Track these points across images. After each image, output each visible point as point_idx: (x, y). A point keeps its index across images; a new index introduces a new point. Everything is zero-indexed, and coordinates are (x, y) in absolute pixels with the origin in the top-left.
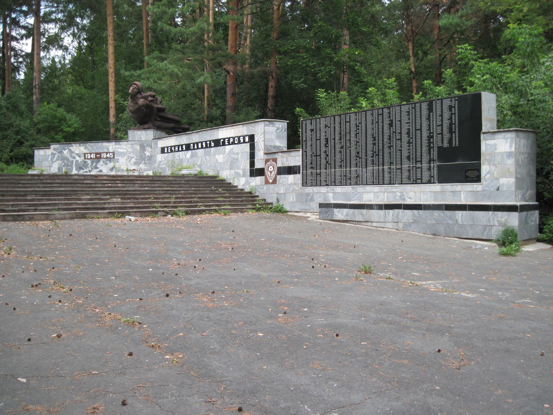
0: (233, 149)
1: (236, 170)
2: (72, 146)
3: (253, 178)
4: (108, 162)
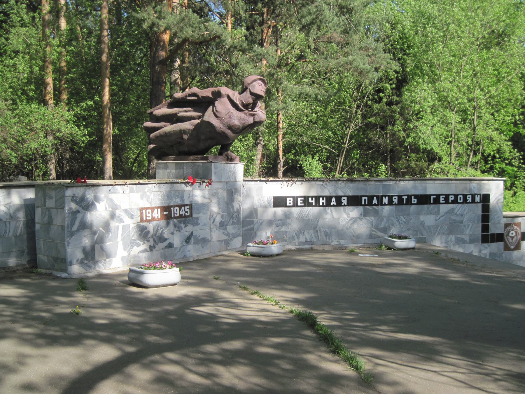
0: (453, 209)
1: (459, 236)
2: (116, 192)
3: (485, 244)
4: (183, 225)
